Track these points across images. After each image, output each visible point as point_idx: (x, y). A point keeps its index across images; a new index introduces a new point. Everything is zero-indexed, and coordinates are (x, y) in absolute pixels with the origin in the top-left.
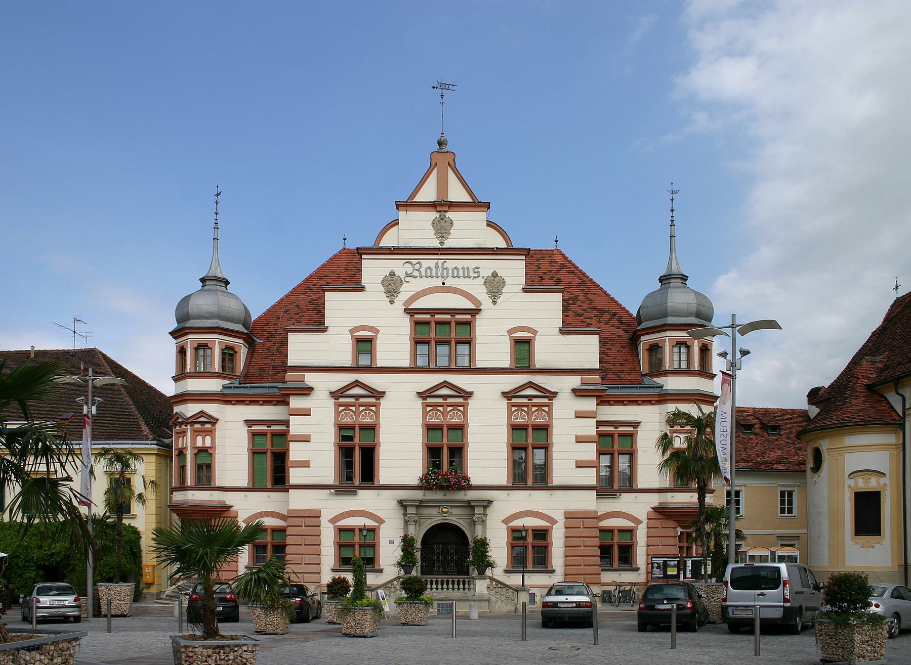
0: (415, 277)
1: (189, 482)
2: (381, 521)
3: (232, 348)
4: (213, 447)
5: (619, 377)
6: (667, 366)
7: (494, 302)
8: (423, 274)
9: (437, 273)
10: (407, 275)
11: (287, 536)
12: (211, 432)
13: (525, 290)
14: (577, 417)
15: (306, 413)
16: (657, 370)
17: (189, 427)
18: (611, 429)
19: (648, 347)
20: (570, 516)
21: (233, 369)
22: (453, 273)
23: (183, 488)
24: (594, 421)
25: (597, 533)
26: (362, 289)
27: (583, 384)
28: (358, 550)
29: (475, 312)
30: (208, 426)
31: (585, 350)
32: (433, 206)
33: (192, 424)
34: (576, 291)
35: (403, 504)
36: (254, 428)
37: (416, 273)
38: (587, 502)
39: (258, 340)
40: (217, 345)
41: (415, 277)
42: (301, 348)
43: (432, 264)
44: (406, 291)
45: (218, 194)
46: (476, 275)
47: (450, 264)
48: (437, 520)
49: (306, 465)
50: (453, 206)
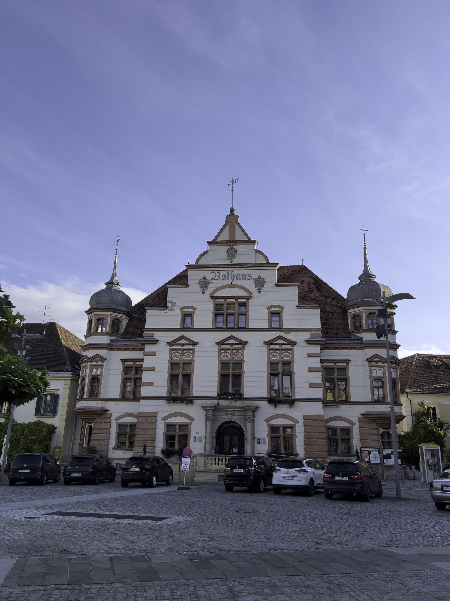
0: (217, 280)
1: (85, 396)
2: (192, 419)
3: (118, 320)
4: (101, 375)
5: (336, 334)
6: (364, 326)
7: (259, 292)
8: (221, 278)
9: (228, 278)
10: (212, 279)
11: (136, 428)
12: (101, 366)
13: (277, 285)
14: (308, 357)
15: (153, 354)
16: (358, 328)
17: (89, 363)
18: (332, 364)
19: (353, 316)
20: (307, 418)
21: (117, 331)
22: (237, 276)
23: (82, 399)
24: (319, 359)
25: (324, 430)
26: (188, 286)
27: (311, 337)
28: (177, 439)
29: (249, 297)
30: (380, 364)
31: (313, 318)
32: (226, 242)
33: (91, 362)
34: (312, 287)
35: (205, 408)
36: (326, 364)
37: (217, 278)
38: (317, 409)
39: (135, 316)
40: (109, 318)
41: (217, 280)
42: (153, 318)
43: (226, 273)
44: (211, 288)
45: (118, 240)
46: (249, 278)
47: (235, 273)
48: (225, 419)
49: (151, 384)
50: (237, 242)
